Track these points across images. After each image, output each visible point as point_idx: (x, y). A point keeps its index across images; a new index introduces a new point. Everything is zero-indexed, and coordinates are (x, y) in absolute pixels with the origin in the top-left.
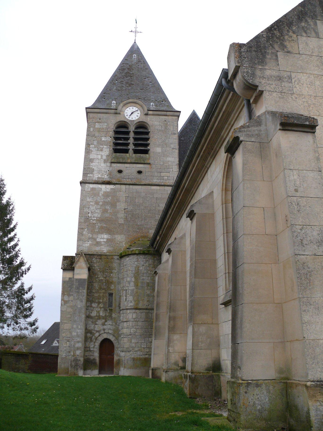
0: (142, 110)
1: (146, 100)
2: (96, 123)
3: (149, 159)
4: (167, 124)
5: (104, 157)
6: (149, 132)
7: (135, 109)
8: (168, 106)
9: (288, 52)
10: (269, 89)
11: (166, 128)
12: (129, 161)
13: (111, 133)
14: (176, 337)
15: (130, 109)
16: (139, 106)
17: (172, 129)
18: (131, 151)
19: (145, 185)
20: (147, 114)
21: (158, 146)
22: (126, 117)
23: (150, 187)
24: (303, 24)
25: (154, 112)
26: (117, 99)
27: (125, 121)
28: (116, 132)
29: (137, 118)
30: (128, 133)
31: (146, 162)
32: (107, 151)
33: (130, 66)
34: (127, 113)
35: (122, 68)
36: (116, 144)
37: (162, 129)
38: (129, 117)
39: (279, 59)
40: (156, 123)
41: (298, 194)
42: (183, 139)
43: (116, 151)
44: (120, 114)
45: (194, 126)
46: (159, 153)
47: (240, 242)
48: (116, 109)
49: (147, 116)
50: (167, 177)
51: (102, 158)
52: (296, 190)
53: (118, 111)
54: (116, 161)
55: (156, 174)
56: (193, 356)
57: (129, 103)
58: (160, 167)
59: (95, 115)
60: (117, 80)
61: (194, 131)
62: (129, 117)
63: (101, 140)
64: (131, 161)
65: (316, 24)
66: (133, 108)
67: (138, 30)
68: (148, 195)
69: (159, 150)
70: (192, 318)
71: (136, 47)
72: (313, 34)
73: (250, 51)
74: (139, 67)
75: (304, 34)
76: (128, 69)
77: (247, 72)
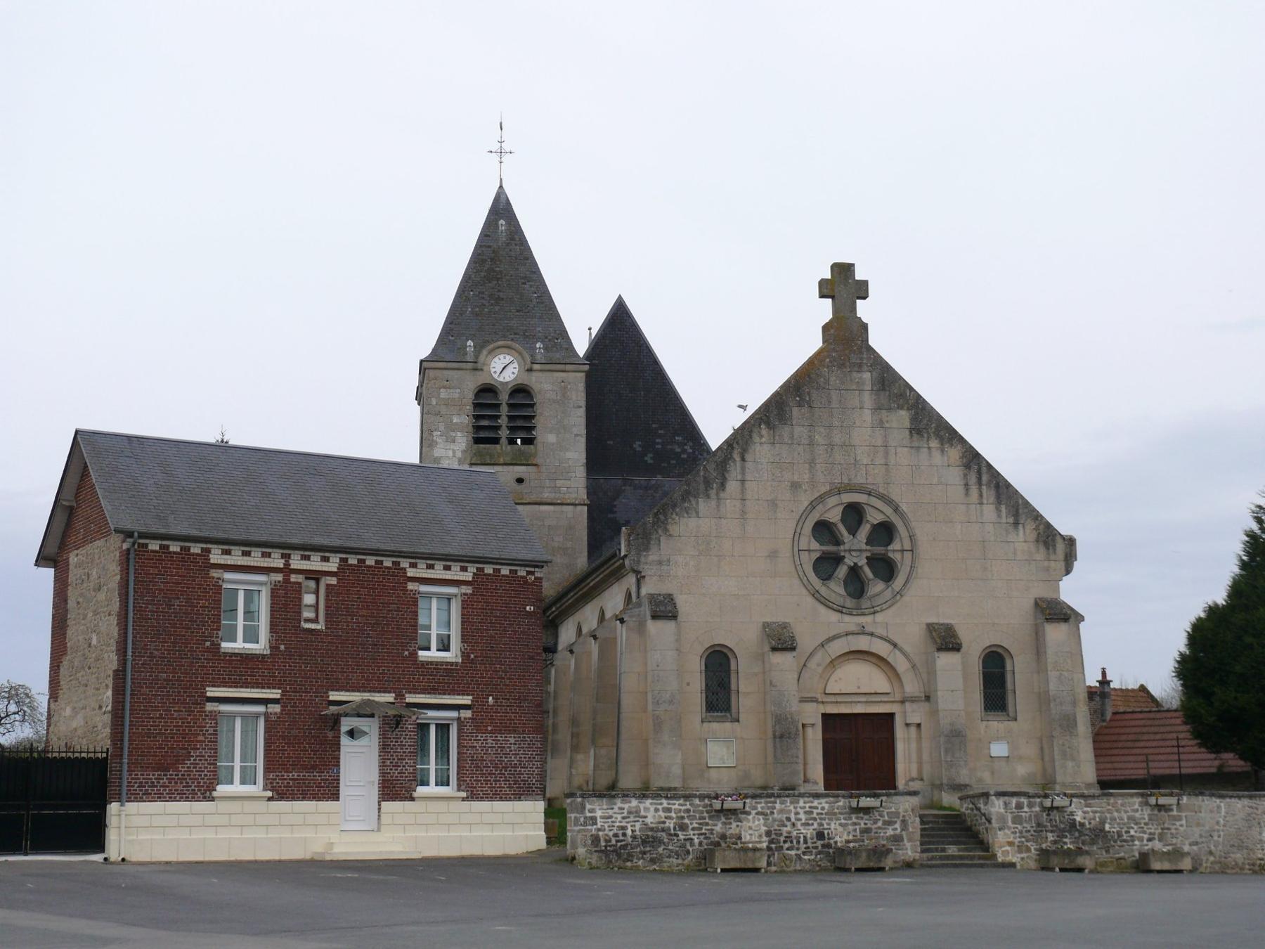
0: (521, 360)
1: (527, 338)
2: (440, 389)
3: (535, 455)
4: (565, 388)
5: (459, 454)
6: (535, 404)
7: (509, 358)
8: (567, 349)
9: (670, 535)
10: (650, 573)
11: (564, 397)
12: (502, 461)
13: (468, 407)
14: (580, 757)
15: (500, 359)
16: (517, 355)
17: (574, 398)
18: (504, 441)
19: (529, 504)
20: (530, 370)
21: (551, 432)
22: (493, 375)
23: (537, 506)
24: (686, 505)
25: (543, 366)
26: (474, 335)
27: (492, 384)
28: (476, 406)
29: (513, 377)
30: (497, 406)
31: (529, 463)
32: (462, 442)
33: (494, 252)
34: (494, 367)
35: (480, 257)
36: (477, 428)
37: (558, 397)
38: (499, 376)
39: (662, 544)
40: (547, 387)
41: (659, 668)
42: (597, 362)
43: (477, 441)
44: (482, 370)
45: (619, 333)
46: (553, 444)
47: (622, 695)
48: (476, 362)
49: (530, 373)
50: (565, 489)
51: (454, 456)
52: (658, 666)
53: (479, 366)
54: (479, 462)
55: (547, 483)
56: (594, 777)
57: (499, 347)
58: (553, 471)
59: (438, 373)
60: (472, 291)
61: (619, 344)
62: (499, 376)
63: (451, 421)
64: (504, 460)
65: (697, 503)
66: (505, 358)
67: (506, 147)
68: (535, 522)
69: (552, 438)
70: (594, 742)
71: (503, 200)
72: (694, 514)
73: (638, 539)
74: (513, 254)
75: (686, 515)
76: (492, 259)
77: (634, 560)
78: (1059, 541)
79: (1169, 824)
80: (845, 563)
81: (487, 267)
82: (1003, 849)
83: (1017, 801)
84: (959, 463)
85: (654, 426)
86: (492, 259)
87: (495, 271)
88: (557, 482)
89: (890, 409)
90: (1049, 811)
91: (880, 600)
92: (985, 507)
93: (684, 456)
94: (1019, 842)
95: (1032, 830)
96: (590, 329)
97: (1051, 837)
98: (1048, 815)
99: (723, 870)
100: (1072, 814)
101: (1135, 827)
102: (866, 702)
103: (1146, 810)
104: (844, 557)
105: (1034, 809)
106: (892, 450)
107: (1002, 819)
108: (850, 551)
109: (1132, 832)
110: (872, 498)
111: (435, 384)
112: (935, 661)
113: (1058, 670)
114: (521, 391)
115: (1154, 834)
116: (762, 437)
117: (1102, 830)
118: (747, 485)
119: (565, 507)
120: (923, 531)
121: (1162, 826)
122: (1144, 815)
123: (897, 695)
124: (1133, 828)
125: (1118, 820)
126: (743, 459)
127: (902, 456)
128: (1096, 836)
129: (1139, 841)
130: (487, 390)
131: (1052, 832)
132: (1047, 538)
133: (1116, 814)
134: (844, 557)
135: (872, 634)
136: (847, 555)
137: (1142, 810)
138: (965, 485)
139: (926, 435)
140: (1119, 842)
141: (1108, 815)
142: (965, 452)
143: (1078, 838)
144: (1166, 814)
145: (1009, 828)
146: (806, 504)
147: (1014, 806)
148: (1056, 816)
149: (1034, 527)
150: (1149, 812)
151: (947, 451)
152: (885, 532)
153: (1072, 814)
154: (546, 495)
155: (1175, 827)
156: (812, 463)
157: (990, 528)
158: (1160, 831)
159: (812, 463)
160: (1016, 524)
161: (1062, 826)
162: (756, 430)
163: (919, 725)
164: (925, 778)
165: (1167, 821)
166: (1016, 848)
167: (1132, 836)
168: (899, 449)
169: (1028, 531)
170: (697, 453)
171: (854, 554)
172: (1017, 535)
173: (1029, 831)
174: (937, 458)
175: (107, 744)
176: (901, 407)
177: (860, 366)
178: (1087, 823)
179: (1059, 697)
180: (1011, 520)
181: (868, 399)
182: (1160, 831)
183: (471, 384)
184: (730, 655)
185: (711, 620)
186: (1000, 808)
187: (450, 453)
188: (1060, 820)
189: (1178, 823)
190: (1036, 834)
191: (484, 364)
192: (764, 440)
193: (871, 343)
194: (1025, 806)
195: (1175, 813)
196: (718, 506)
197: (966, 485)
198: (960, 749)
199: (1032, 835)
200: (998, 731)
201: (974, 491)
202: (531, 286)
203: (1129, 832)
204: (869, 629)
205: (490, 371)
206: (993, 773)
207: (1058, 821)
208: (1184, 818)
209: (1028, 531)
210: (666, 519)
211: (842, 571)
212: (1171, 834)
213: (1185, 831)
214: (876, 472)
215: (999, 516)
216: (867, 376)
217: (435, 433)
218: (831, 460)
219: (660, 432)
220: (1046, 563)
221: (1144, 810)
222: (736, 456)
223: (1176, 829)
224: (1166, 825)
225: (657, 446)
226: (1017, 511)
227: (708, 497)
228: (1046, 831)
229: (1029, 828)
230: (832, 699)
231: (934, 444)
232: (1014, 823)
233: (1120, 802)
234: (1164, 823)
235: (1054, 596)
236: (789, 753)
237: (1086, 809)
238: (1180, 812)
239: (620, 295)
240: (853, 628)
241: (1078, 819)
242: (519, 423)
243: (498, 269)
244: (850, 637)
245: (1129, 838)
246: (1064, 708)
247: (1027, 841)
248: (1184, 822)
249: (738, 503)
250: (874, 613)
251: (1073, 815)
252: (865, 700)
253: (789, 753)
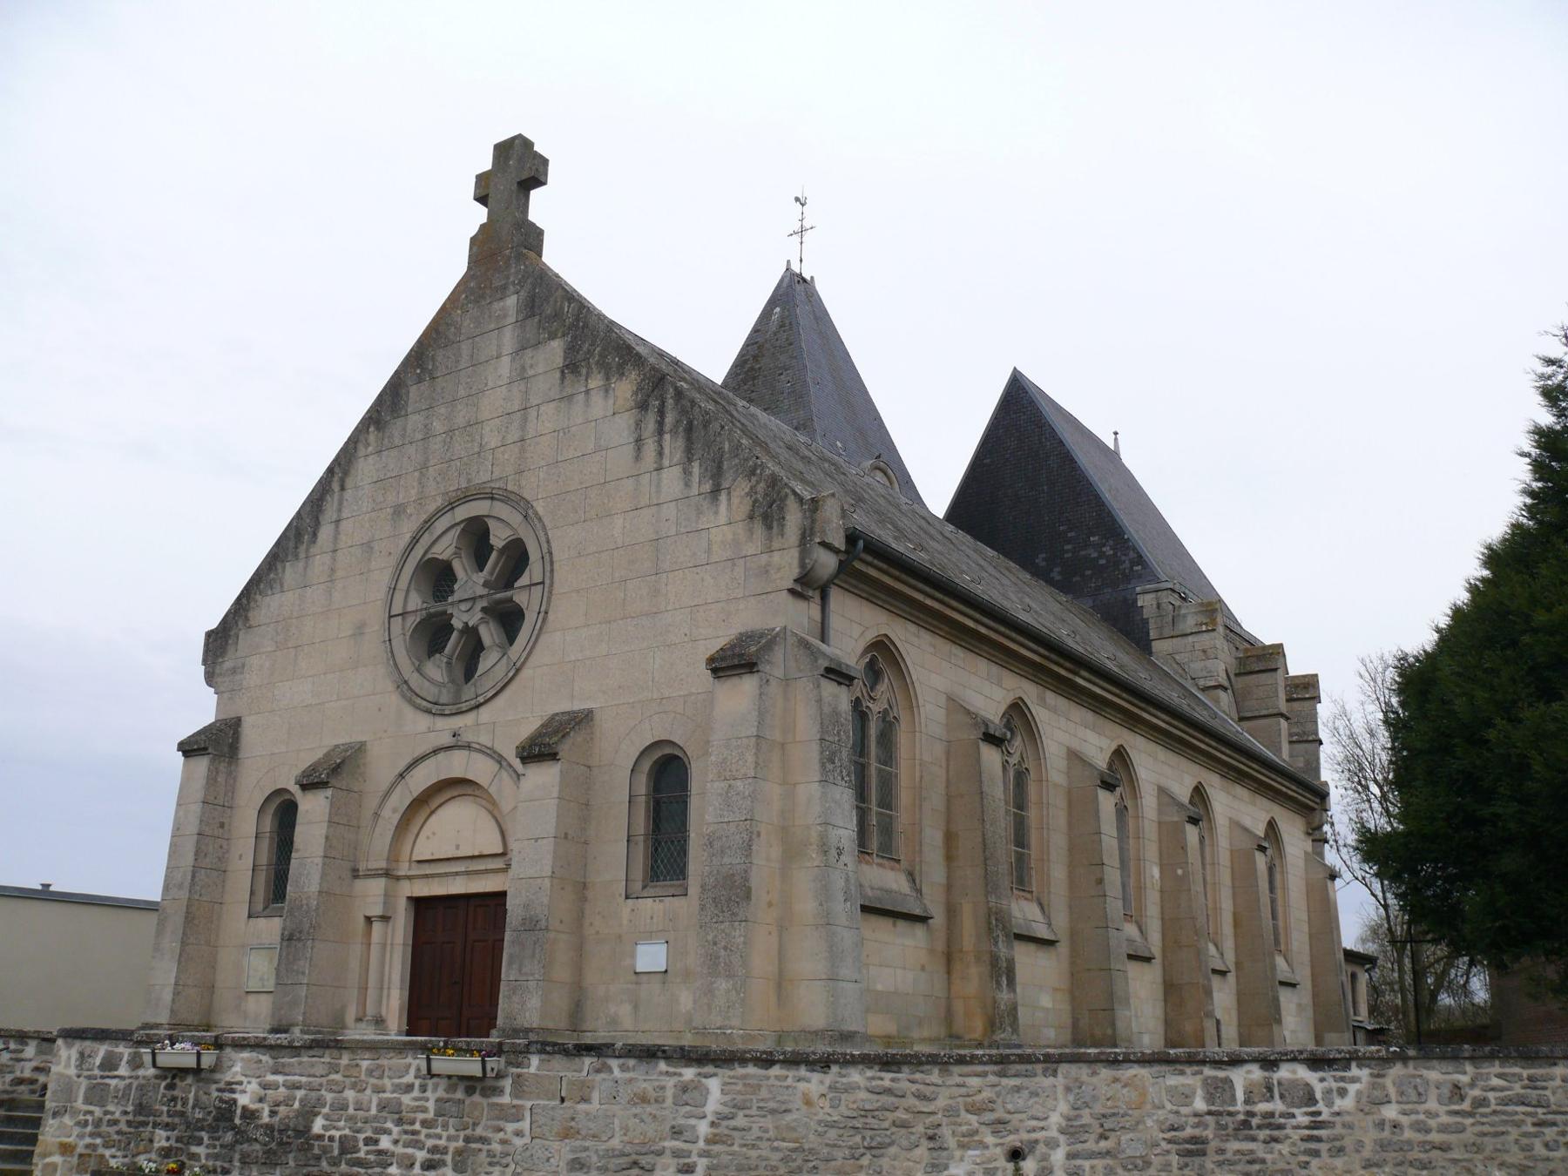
65: (284, 568)
75: (270, 593)
79: (486, 1128)
82: (48, 1160)
83: (107, 1051)
85: (1061, 528)
90: (174, 1077)
92: (665, 474)
93: (1102, 562)
94: (88, 1146)
95: (124, 1119)
96: (1116, 433)
97: (161, 1139)
98: (171, 1087)
100: (230, 1087)
101: (396, 1130)
102: (467, 873)
103: (435, 1089)
105: (141, 1072)
107: (68, 1090)
109: (385, 1143)
110: (497, 503)
113: (726, 779)
115: (445, 1151)
117: (304, 1132)
121: (469, 1132)
122: (427, 1100)
124: (388, 1132)
125: (351, 1111)
126: (343, 488)
128: (281, 1144)
129: (400, 1166)
131: (167, 1126)
132: (770, 506)
133: (350, 1095)
137: (423, 1089)
138: (637, 441)
139: (584, 371)
140: (324, 1164)
141: (329, 1097)
142: (643, 380)
143: (231, 1147)
144: (484, 1102)
145: (75, 1112)
147: (98, 1061)
148: (189, 1090)
149: (747, 490)
150: (441, 1093)
151: (614, 389)
152: (517, 557)
153: (230, 1087)
155: (501, 1135)
157: (670, 511)
158: (461, 1143)
160: (715, 492)
161: (199, 1115)
165: (483, 1122)
166: (75, 1160)
167: (380, 1152)
170: (1119, 554)
172: (716, 513)
173: (115, 1122)
174: (599, 407)
178: (266, 1113)
179: (720, 838)
182: (461, 1143)
185: (277, 751)
186: (68, 1065)
188: (196, 1099)
189: (511, 1127)
190: (132, 1130)
192: (370, 449)
194: (123, 1063)
195: (506, 1099)
196: (305, 568)
198: (533, 956)
199: (118, 1133)
200: (652, 918)
203: (376, 1142)
204: (467, 737)
206: (636, 1007)
207: (191, 1102)
208: (527, 1114)
209: (735, 501)
210: (249, 603)
212: (490, 1154)
213: (526, 1148)
214: (506, 457)
215: (687, 485)
218: (449, 454)
219: (1069, 535)
220: (765, 557)
221: (430, 1088)
222: (336, 486)
223: (504, 1142)
224: (479, 1131)
225: (1066, 556)
226: (720, 467)
227: (296, 557)
228: (155, 1125)
229: (117, 1115)
230: (428, 869)
231: (596, 382)
232: (87, 1101)
233: (365, 1064)
234: (475, 1125)
236: (295, 967)
237: (271, 1078)
238: (517, 1097)
239: (1015, 368)
240: (447, 740)
241: (243, 1100)
244: (441, 756)
245: (372, 1157)
246: (726, 860)
247: (106, 1146)
248: (525, 1125)
251: (233, 1091)
253: (295, 967)
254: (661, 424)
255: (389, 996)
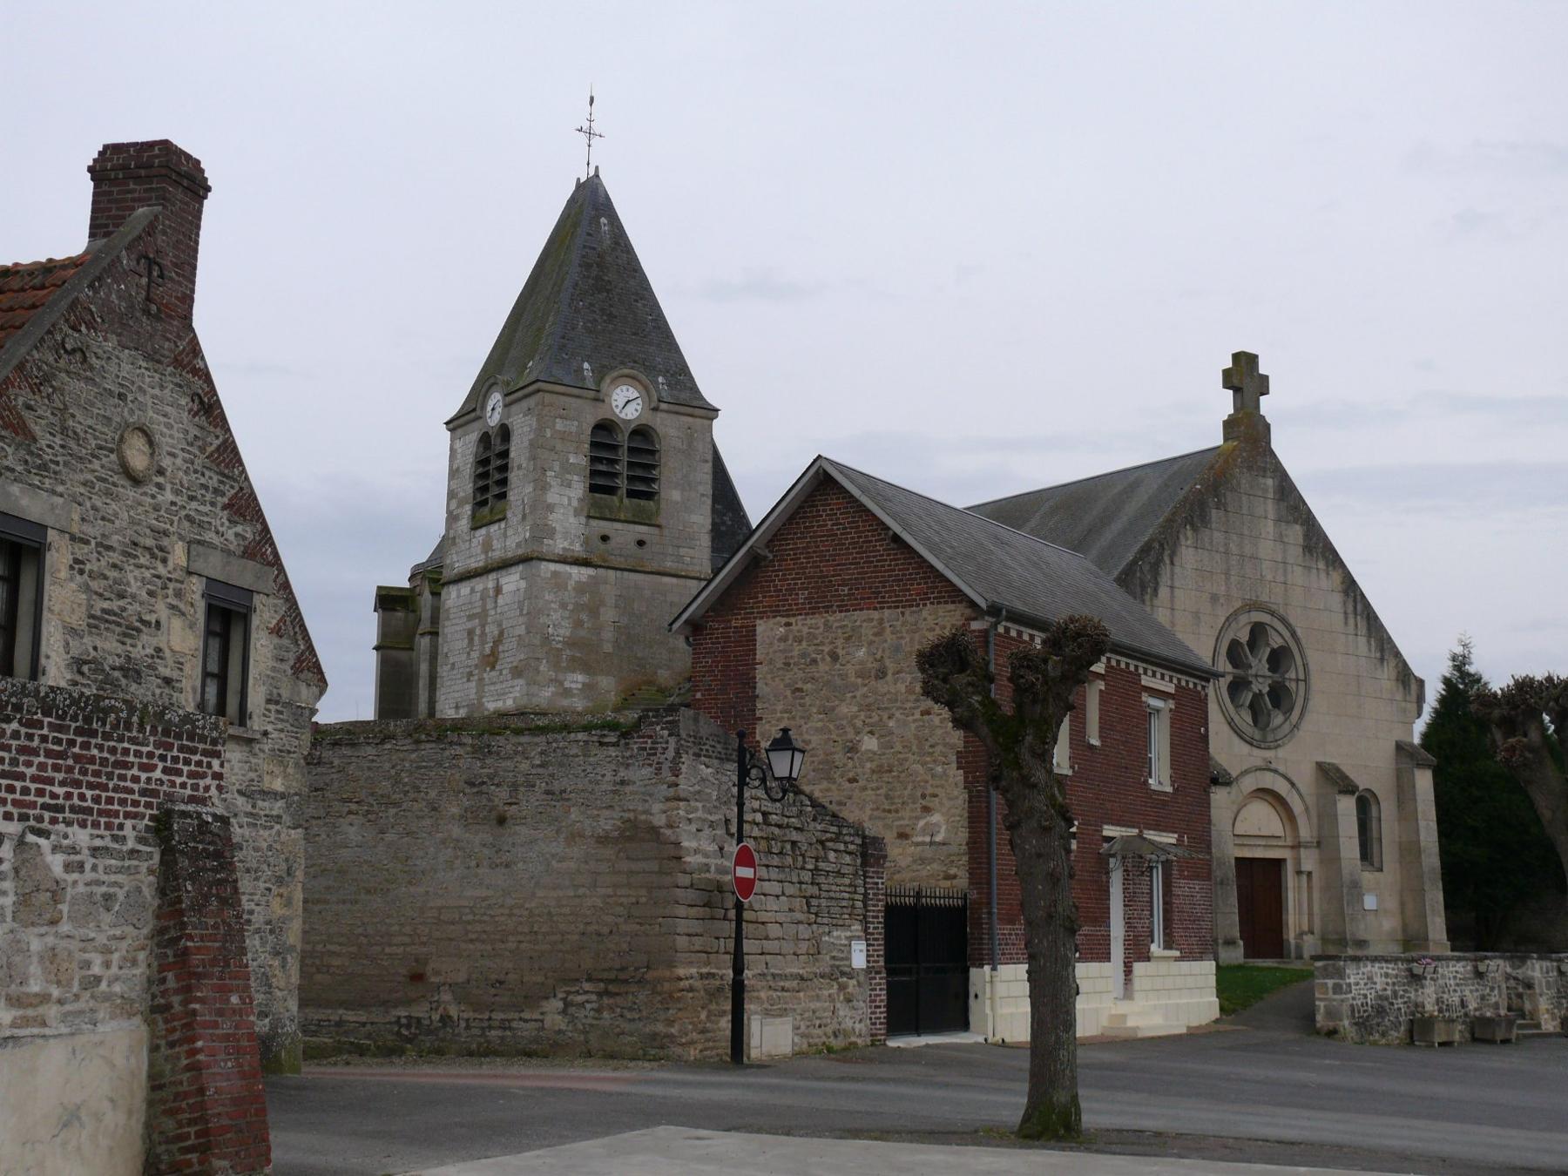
1: (651, 370)
5: (575, 503)
8: (691, 389)
20: (655, 409)
25: (671, 406)
36: (593, 473)
38: (621, 412)
40: (672, 432)
43: (593, 488)
44: (603, 401)
51: (570, 504)
55: (670, 550)
57: (622, 376)
62: (621, 412)
63: (568, 460)
69: (676, 495)
74: (620, 262)
78: (1413, 681)
80: (1250, 690)
81: (594, 274)
84: (1340, 589)
86: (598, 266)
87: (603, 280)
88: (681, 550)
89: (1288, 522)
91: (1280, 734)
93: (723, 528)
99: (1440, 1044)
102: (1265, 846)
104: (1251, 682)
106: (1289, 567)
108: (1256, 676)
111: (550, 411)
112: (1335, 804)
114: (642, 432)
116: (1187, 539)
118: (1177, 592)
119: (666, 579)
120: (1313, 658)
123: (1288, 839)
126: (1172, 563)
127: (1297, 576)
130: (605, 427)
134: (1251, 682)
135: (1275, 771)
136: (1254, 681)
146: (1223, 619)
154: (669, 564)
156: (1227, 574)
159: (1227, 574)
160: (1382, 659)
162: (1182, 530)
163: (1309, 874)
164: (1315, 931)
168: (1295, 568)
169: (1391, 669)
171: (1260, 680)
172: (1383, 671)
175: (962, 882)
176: (1296, 522)
177: (1264, 469)
180: (1378, 655)
181: (1271, 508)
183: (590, 421)
184: (1372, 800)
187: (566, 501)
191: (606, 395)
192: (1189, 542)
193: (1273, 446)
197: (1345, 613)
201: (1351, 621)
202: (644, 305)
205: (611, 404)
211: (1247, 698)
215: (1370, 650)
216: (1270, 482)
217: (549, 473)
220: (1403, 704)
231: (1321, 565)
235: (1409, 740)
240: (1259, 763)
242: (639, 473)
243: (606, 278)
244: (1258, 772)
249: (1168, 612)
250: (1276, 748)
252: (1264, 843)
254: (1355, 608)
255: (1311, 914)
